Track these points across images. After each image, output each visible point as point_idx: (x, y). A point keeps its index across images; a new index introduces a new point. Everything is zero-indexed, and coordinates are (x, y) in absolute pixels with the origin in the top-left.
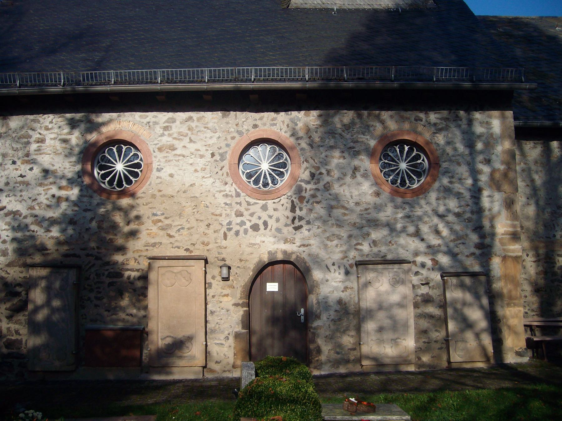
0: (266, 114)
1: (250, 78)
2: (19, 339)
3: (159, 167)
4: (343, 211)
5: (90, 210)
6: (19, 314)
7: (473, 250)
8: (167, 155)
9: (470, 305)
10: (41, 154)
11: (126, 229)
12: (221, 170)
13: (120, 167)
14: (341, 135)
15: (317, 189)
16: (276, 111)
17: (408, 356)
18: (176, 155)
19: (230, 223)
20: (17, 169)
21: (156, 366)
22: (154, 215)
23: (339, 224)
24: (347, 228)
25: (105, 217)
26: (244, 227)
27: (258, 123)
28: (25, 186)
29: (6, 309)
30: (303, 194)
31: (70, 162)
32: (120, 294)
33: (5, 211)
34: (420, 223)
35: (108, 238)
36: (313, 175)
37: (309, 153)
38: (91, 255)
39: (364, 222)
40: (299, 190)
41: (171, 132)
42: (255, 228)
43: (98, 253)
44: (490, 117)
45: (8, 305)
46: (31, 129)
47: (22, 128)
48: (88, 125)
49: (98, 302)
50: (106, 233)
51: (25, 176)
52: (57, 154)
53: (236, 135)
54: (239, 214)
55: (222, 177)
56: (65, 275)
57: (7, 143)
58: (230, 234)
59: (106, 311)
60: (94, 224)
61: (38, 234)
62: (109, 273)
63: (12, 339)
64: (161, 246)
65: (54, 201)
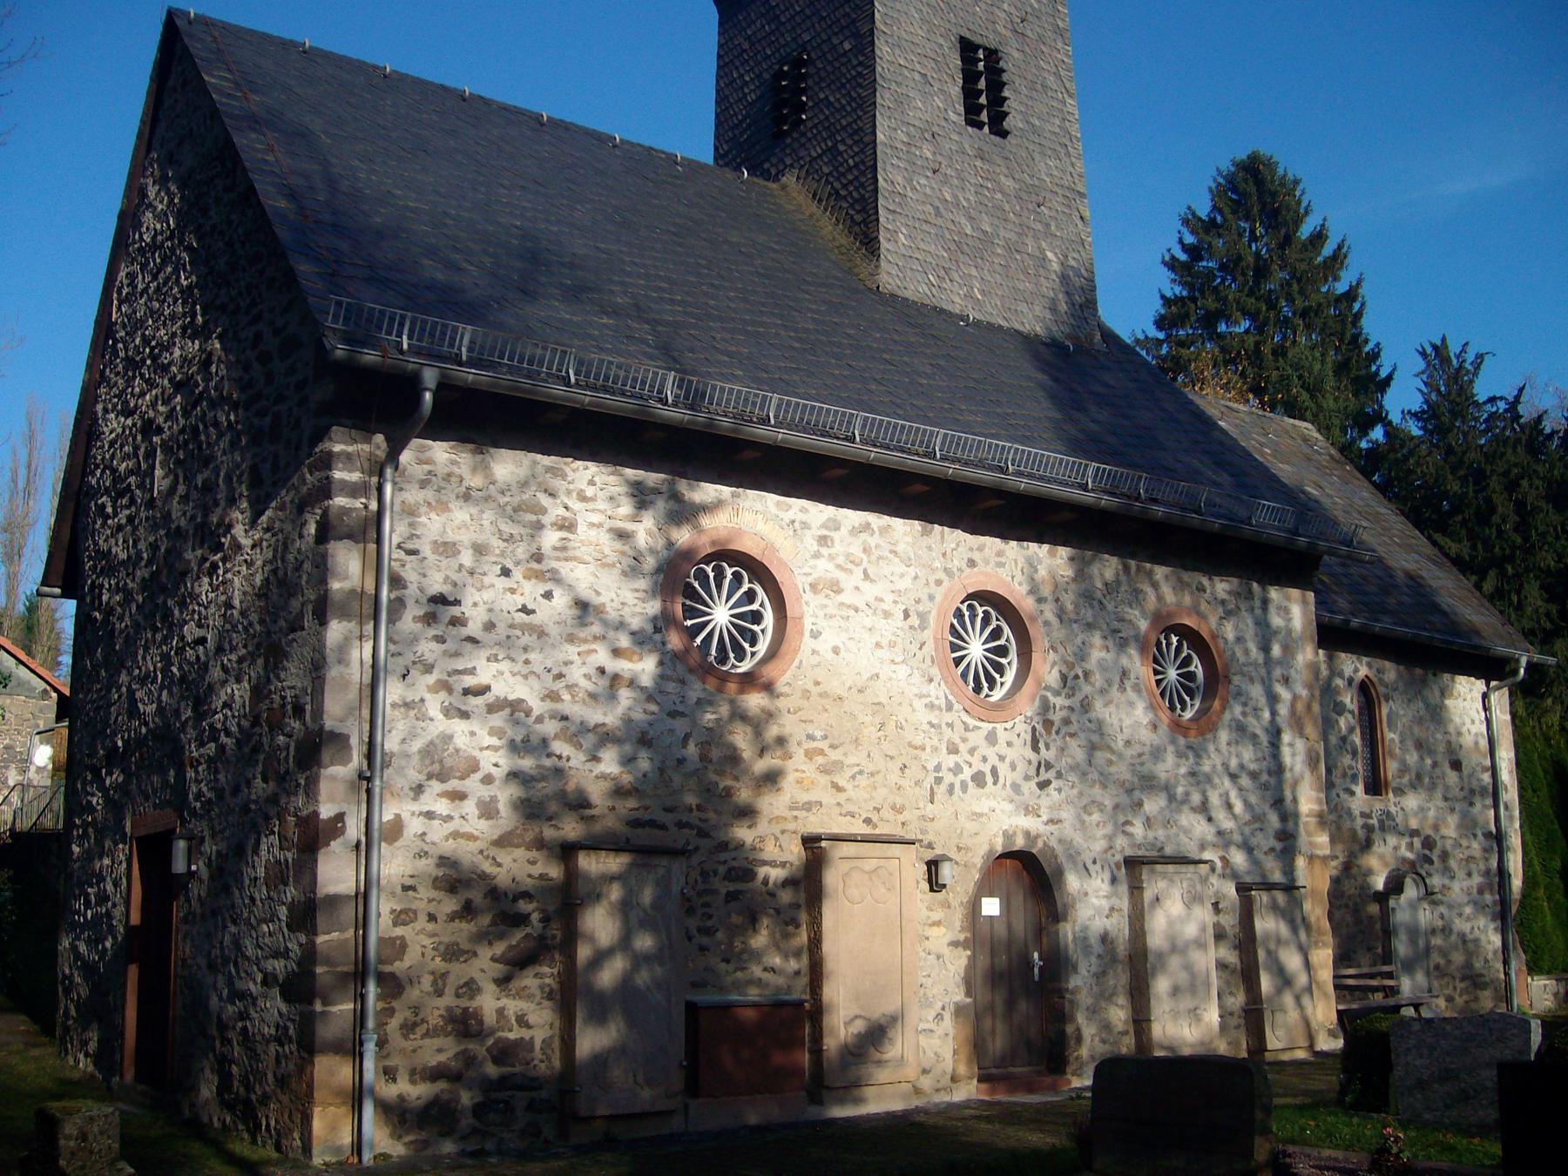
1: (456, 351)
2: (527, 1038)
3: (814, 628)
4: (1109, 755)
5: (682, 714)
6: (525, 972)
7: (1273, 842)
8: (826, 601)
9: (1287, 943)
10: (566, 559)
11: (761, 766)
12: (920, 648)
13: (721, 615)
14: (1100, 602)
15: (1071, 709)
16: (1004, 537)
17: (1211, 1042)
18: (842, 604)
19: (938, 768)
20: (513, 591)
21: (838, 1085)
22: (811, 737)
23: (1105, 781)
24: (1113, 790)
25: (713, 737)
26: (961, 777)
27: (976, 556)
28: (535, 636)
29: (493, 959)
30: (1051, 716)
31: (637, 591)
32: (753, 922)
33: (489, 698)
34: (1208, 787)
35: (721, 786)
36: (1064, 678)
37: (1059, 633)
38: (688, 825)
39: (1136, 780)
40: (1045, 707)
41: (833, 551)
42: (979, 779)
44: (1288, 598)
45: (499, 948)
46: (546, 491)
47: (524, 485)
48: (672, 505)
49: (705, 940)
50: (716, 772)
51: (533, 612)
52: (605, 565)
53: (941, 575)
54: (953, 750)
55: (924, 666)
56: (661, 871)
57: (485, 516)
59: (723, 960)
60: (692, 750)
61: (571, 764)
62: (730, 870)
63: (507, 1039)
64: (821, 810)
65: (604, 682)
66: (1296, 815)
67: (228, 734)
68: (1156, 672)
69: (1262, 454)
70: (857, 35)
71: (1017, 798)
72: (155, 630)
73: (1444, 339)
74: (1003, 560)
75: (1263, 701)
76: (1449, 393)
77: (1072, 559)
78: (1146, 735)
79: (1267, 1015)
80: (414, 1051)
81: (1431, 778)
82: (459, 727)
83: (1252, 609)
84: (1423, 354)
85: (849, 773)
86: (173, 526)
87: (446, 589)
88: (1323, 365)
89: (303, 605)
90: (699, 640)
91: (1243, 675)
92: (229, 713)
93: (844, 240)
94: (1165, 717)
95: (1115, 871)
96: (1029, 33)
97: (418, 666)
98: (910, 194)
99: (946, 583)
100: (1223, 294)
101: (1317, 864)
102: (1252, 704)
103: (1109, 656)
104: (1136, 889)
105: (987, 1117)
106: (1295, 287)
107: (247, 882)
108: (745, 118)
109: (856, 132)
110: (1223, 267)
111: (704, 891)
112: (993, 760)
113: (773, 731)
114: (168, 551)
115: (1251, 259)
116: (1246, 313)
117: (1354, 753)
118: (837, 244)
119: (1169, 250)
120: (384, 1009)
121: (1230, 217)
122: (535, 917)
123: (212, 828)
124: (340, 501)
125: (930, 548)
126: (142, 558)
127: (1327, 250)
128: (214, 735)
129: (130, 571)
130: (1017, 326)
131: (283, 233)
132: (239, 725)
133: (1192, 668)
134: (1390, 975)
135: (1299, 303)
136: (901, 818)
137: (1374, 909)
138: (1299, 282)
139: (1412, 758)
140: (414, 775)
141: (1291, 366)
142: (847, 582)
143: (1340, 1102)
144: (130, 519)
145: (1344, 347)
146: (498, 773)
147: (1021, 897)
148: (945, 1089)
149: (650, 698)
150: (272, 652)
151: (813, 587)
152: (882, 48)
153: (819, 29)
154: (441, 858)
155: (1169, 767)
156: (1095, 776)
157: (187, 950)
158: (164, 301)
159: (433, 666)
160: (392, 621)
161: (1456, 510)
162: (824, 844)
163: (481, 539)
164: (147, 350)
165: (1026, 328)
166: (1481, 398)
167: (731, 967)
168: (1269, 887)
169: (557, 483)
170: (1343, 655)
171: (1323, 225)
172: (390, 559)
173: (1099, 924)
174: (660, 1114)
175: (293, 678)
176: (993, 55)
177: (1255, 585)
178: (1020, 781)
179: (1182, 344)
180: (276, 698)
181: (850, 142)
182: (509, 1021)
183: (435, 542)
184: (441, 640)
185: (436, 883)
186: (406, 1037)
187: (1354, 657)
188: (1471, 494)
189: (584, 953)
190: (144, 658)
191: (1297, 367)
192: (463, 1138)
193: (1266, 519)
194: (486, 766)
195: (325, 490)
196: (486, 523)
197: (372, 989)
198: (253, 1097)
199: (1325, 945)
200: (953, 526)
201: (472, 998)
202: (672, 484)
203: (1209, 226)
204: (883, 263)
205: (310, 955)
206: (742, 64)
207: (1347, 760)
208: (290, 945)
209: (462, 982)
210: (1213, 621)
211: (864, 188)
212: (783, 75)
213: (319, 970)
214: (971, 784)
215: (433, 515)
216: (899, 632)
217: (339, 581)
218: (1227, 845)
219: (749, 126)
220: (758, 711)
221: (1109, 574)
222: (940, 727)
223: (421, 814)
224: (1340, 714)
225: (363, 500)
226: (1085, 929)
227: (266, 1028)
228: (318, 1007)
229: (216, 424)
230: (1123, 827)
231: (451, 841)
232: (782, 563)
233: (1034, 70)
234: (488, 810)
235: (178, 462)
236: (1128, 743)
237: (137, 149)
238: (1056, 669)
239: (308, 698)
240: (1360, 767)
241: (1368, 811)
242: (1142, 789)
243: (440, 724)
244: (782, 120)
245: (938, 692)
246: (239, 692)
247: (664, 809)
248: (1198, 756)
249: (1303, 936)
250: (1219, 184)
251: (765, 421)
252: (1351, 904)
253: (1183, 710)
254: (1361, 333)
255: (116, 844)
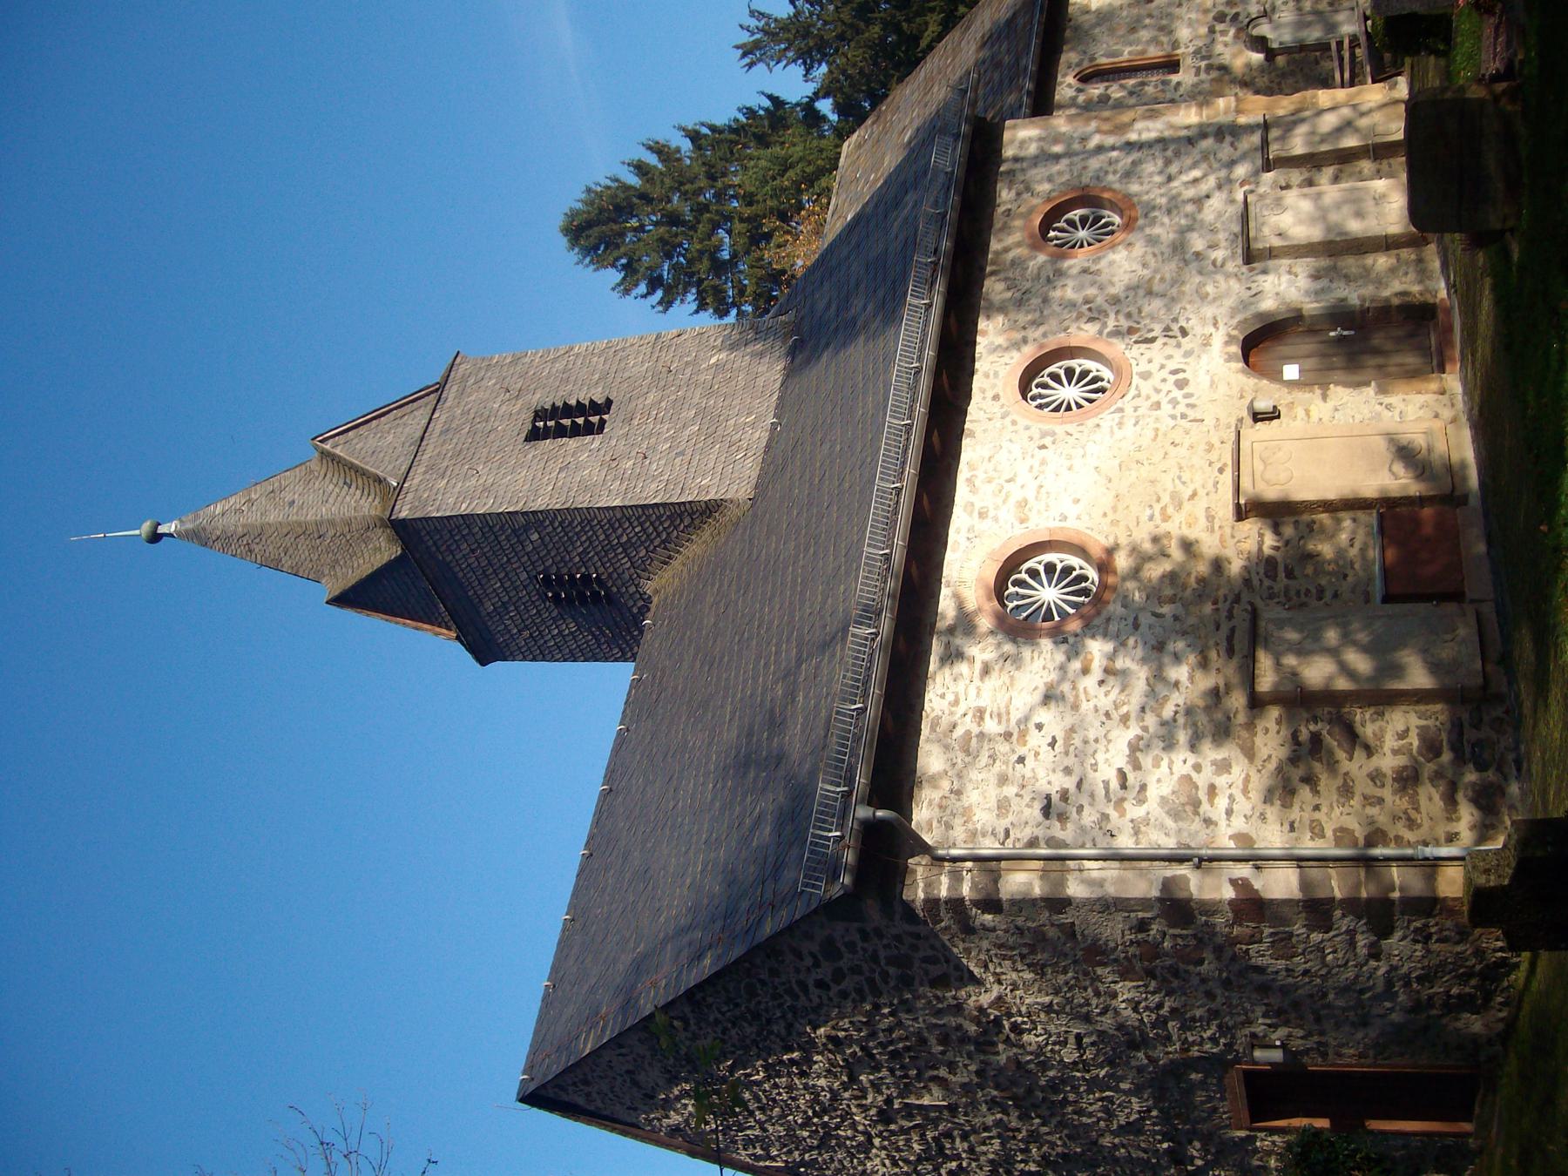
0: (975, 386)
1: (839, 796)
4: (1156, 281)
5: (1136, 618)
9: (1314, 126)
11: (1177, 554)
13: (1049, 594)
15: (1117, 312)
18: (1036, 498)
19: (1173, 417)
20: (1037, 754)
22: (1151, 518)
23: (1177, 281)
25: (1154, 593)
26: (1180, 399)
27: (990, 394)
28: (1074, 735)
29: (1351, 759)
31: (1032, 658)
32: (1311, 557)
33: (1128, 769)
35: (1195, 586)
36: (1091, 320)
37: (1053, 323)
40: (1117, 333)
43: (1225, 601)
44: (1012, 141)
45: (1341, 755)
46: (951, 731)
47: (947, 747)
48: (958, 632)
51: (1054, 738)
52: (1012, 684)
53: (1008, 420)
54: (1157, 406)
56: (1271, 627)
57: (974, 778)
58: (1192, 414)
60: (1165, 609)
61: (1181, 703)
62: (1267, 576)
63: (1418, 747)
65: (1111, 680)
66: (1200, 125)
67: (1160, 1006)
68: (1082, 246)
69: (876, 180)
70: (526, 528)
71: (1196, 353)
72: (1065, 1102)
73: (737, 47)
74: (992, 373)
75: (1102, 157)
76: (788, 40)
77: (988, 317)
78: (1139, 249)
79: (1379, 140)
80: (1431, 819)
81: (1161, 18)
82: (1153, 793)
83: (1023, 170)
84: (751, 65)
85: (1180, 487)
86: (976, 1080)
87: (1038, 806)
88: (762, 159)
89: (1053, 925)
90: (1071, 611)
91: (1080, 176)
92: (1143, 1004)
93: (706, 534)
94: (1119, 236)
95: (1256, 272)
96: (518, 386)
97: (1103, 824)
98: (666, 477)
99: (1015, 417)
100: (695, 254)
101: (1242, 106)
102: (1105, 165)
103: (1071, 283)
104: (1272, 253)
105: (1472, 355)
106: (688, 187)
107: (1290, 980)
108: (593, 634)
109: (612, 526)
110: (669, 256)
111: (1285, 596)
112: (1164, 373)
113: (1147, 546)
114: (997, 1087)
115: (662, 230)
116: (710, 235)
117: (1143, 84)
118: (710, 539)
119: (653, 307)
120: (1396, 843)
121: (622, 250)
122: (1312, 727)
123: (1243, 1024)
124: (966, 890)
125: (985, 431)
126: (1001, 1120)
127: (652, 160)
128: (1161, 1023)
129: (1011, 1134)
130: (778, 385)
131: (738, 951)
132: (1153, 993)
133: (1077, 218)
134: (1340, 44)
135: (703, 182)
136: (1217, 444)
137: (1281, 60)
138: (682, 184)
139: (1145, 35)
140: (1197, 825)
141: (763, 187)
142: (1017, 494)
143: (1444, 54)
144: (965, 1137)
145: (743, 140)
146: (1192, 759)
147: (1280, 348)
148: (1451, 400)
149: (1123, 644)
150: (1096, 953)
151: (1022, 521)
152: (539, 504)
153: (517, 564)
154: (1265, 802)
155: (1164, 230)
156: (1174, 291)
157: (1352, 1051)
158: (774, 1100)
159: (1103, 814)
160: (1066, 846)
161: (897, 29)
162: (1242, 501)
163: (993, 780)
164: (815, 1120)
165: (779, 378)
166: (791, 11)
167: (1350, 573)
168: (1265, 143)
169: (945, 721)
170: (1057, 97)
171: (629, 165)
172: (1014, 848)
173: (1303, 282)
174: (1479, 621)
175: (1114, 931)
176: (540, 414)
177: (1002, 169)
178: (1181, 351)
179: (742, 292)
180: (1132, 950)
181: (620, 531)
182: (1403, 746)
183: (998, 815)
184: (1080, 809)
185: (1287, 805)
186: (1420, 826)
187: (1058, 88)
188: (882, 15)
189: (1342, 684)
190: (1090, 1115)
191: (764, 182)
192: (1506, 779)
193: (947, 159)
194: (1187, 769)
195: (956, 904)
196: (980, 777)
197: (1378, 851)
198: (1478, 967)
199: (1315, 96)
200: (965, 413)
201: (1385, 776)
202: (940, 633)
203: (630, 269)
204: (729, 496)
205: (1352, 905)
206: (543, 637)
207: (1150, 89)
208: (1344, 929)
209: (1371, 783)
210: (1036, 201)
211: (662, 516)
212: (556, 596)
213: (1364, 895)
214: (1186, 390)
215: (975, 819)
216: (1059, 451)
217: (1033, 889)
218: (1229, 181)
219: (599, 628)
220: (1130, 560)
221: (1000, 286)
222: (1138, 417)
223: (1228, 819)
224: (1109, 98)
225: (965, 873)
226: (1307, 293)
227: (1418, 954)
228: (1396, 895)
229: (890, 1030)
230: (1217, 267)
231: (1250, 795)
232: (1004, 545)
233: (551, 380)
234: (1223, 767)
235: (919, 1077)
236: (1144, 265)
237: (636, 1137)
238: (1083, 326)
239: (1133, 915)
240: (1154, 78)
241: (1194, 70)
242: (1184, 253)
243: (1152, 806)
244: (596, 595)
245: (1107, 419)
246: (1126, 991)
247: (1217, 630)
248: (1154, 208)
249: (1307, 113)
250: (592, 262)
251: (887, 558)
252: (1277, 80)
253: (1113, 224)
254: (730, 127)
255: (1256, 1151)
